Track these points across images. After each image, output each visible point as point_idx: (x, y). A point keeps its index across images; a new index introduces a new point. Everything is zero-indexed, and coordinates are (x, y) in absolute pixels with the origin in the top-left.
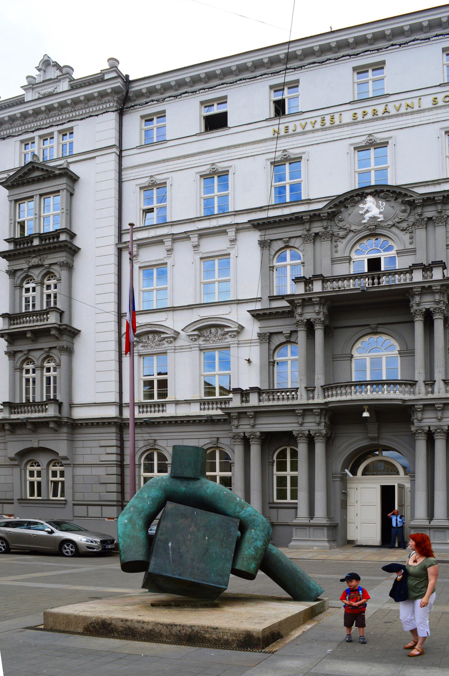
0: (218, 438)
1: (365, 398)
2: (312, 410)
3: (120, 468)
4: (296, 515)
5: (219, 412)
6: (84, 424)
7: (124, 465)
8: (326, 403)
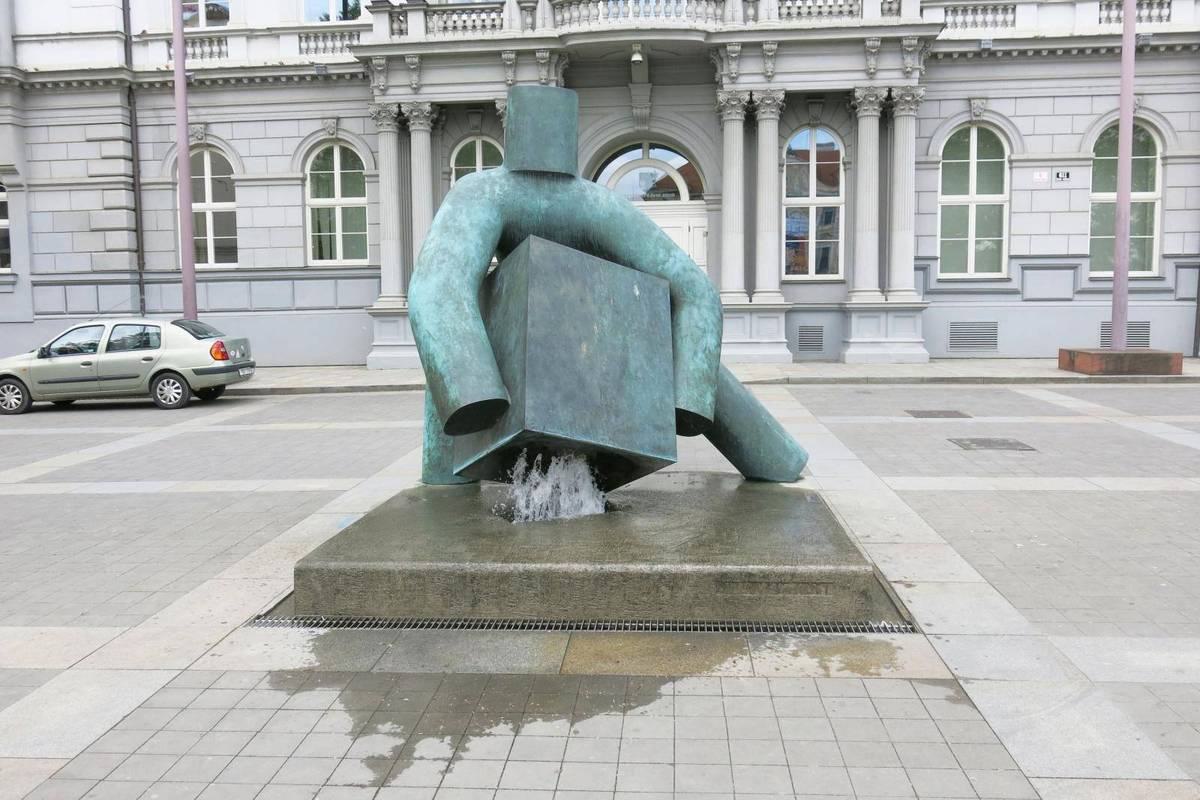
0: (338, 119)
1: (594, 30)
2: (533, 52)
3: (132, 193)
4: (380, 292)
5: (349, 57)
6: (50, 86)
7: (140, 185)
8: (562, 38)
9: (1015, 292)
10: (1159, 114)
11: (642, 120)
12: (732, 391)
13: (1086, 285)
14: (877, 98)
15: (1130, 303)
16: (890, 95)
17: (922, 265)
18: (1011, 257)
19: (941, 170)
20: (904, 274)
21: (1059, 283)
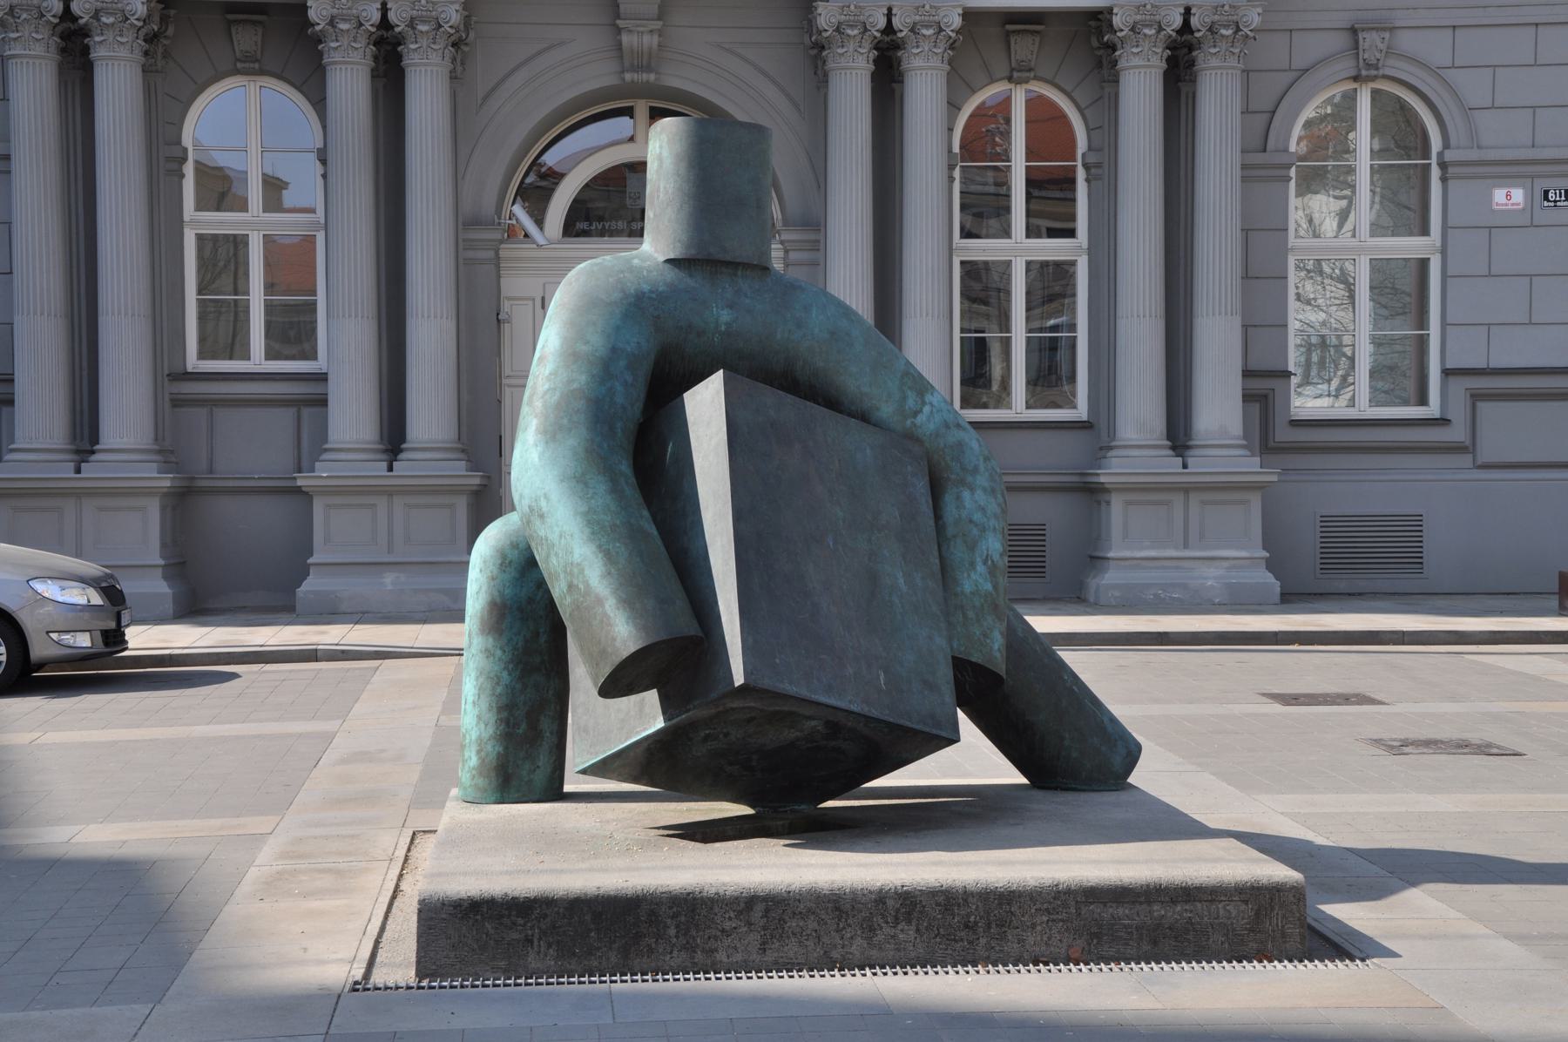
11: (644, 63)
12: (497, 680)
14: (1160, 29)
19: (1293, 184)
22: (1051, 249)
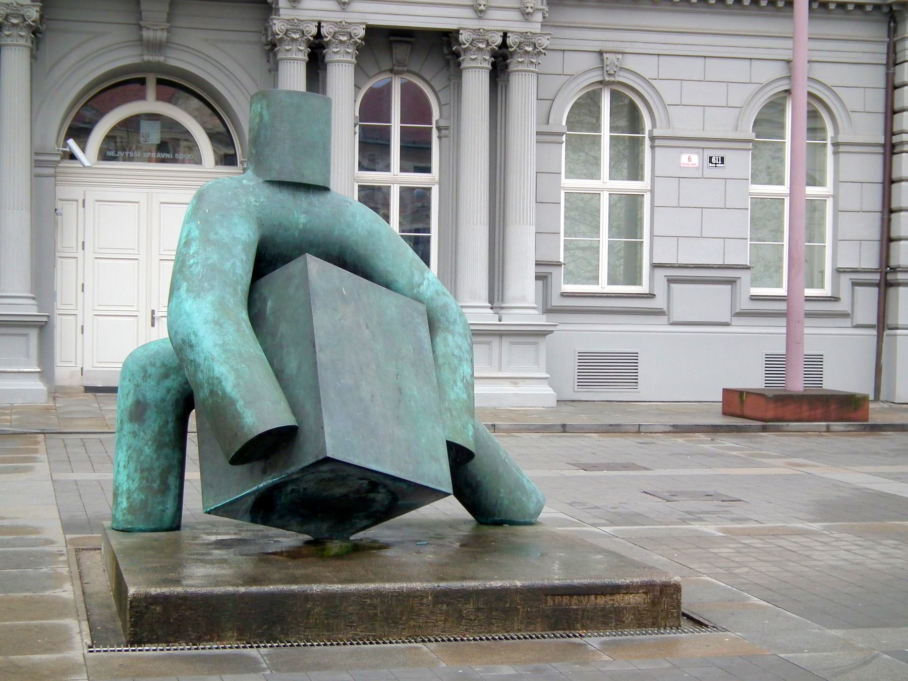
9: (658, 313)
10: (829, 88)
11: (158, 47)
13: (746, 305)
15: (806, 331)
16: (504, 41)
17: (544, 273)
18: (655, 266)
19: (564, 145)
20: (522, 286)
21: (712, 301)
22: (416, 179)
